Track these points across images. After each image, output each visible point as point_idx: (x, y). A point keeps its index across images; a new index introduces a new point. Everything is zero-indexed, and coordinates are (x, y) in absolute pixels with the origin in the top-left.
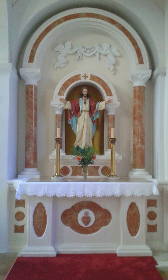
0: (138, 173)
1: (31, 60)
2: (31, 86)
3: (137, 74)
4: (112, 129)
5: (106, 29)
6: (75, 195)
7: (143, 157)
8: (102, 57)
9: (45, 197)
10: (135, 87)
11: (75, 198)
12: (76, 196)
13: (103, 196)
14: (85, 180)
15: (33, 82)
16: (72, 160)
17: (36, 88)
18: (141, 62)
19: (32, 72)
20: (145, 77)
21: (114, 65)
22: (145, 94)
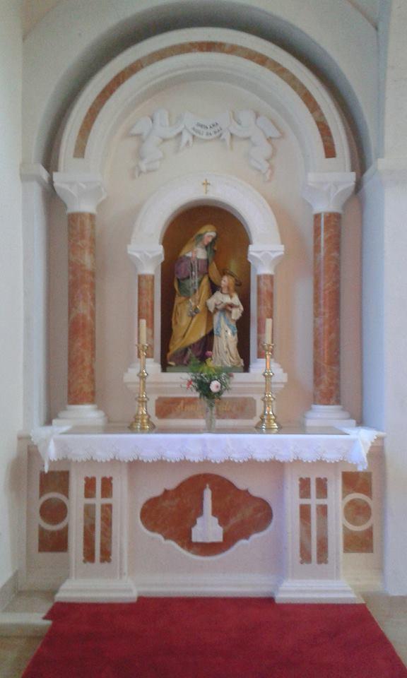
0: (323, 414)
1: (80, 151)
2: (80, 215)
3: (325, 184)
4: (269, 322)
7: (336, 377)
9: (114, 462)
10: (317, 217)
11: (184, 463)
12: (117, 458)
13: (317, 460)
14: (210, 429)
15: (86, 206)
16: (179, 382)
17: (92, 216)
18: (330, 152)
19: (81, 183)
20: (340, 189)
21: (268, 160)
22: (336, 245)
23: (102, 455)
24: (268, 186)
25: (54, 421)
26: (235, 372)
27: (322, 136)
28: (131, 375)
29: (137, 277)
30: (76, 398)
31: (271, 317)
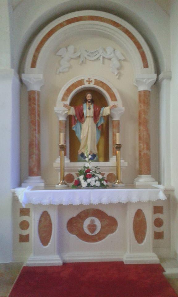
0: (143, 179)
1: (33, 65)
2: (33, 92)
4: (117, 134)
7: (148, 163)
9: (51, 205)
10: (140, 92)
11: (81, 205)
15: (36, 88)
18: (146, 66)
19: (35, 78)
23: (46, 202)
24: (114, 67)
25: (23, 184)
26: (94, 105)
27: (128, 35)
28: (57, 163)
29: (61, 55)
30: (31, 173)
31: (118, 132)
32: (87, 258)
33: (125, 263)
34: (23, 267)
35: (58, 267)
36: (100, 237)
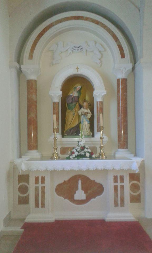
1: (31, 57)
3: (119, 68)
4: (101, 115)
5: (62, 28)
6: (55, 169)
8: (80, 53)
9: (46, 171)
11: (72, 171)
15: (33, 77)
18: (123, 56)
19: (31, 69)
32: (129, 218)
33: (106, 221)
34: (95, 146)
35: (54, 222)
36: (81, 202)
